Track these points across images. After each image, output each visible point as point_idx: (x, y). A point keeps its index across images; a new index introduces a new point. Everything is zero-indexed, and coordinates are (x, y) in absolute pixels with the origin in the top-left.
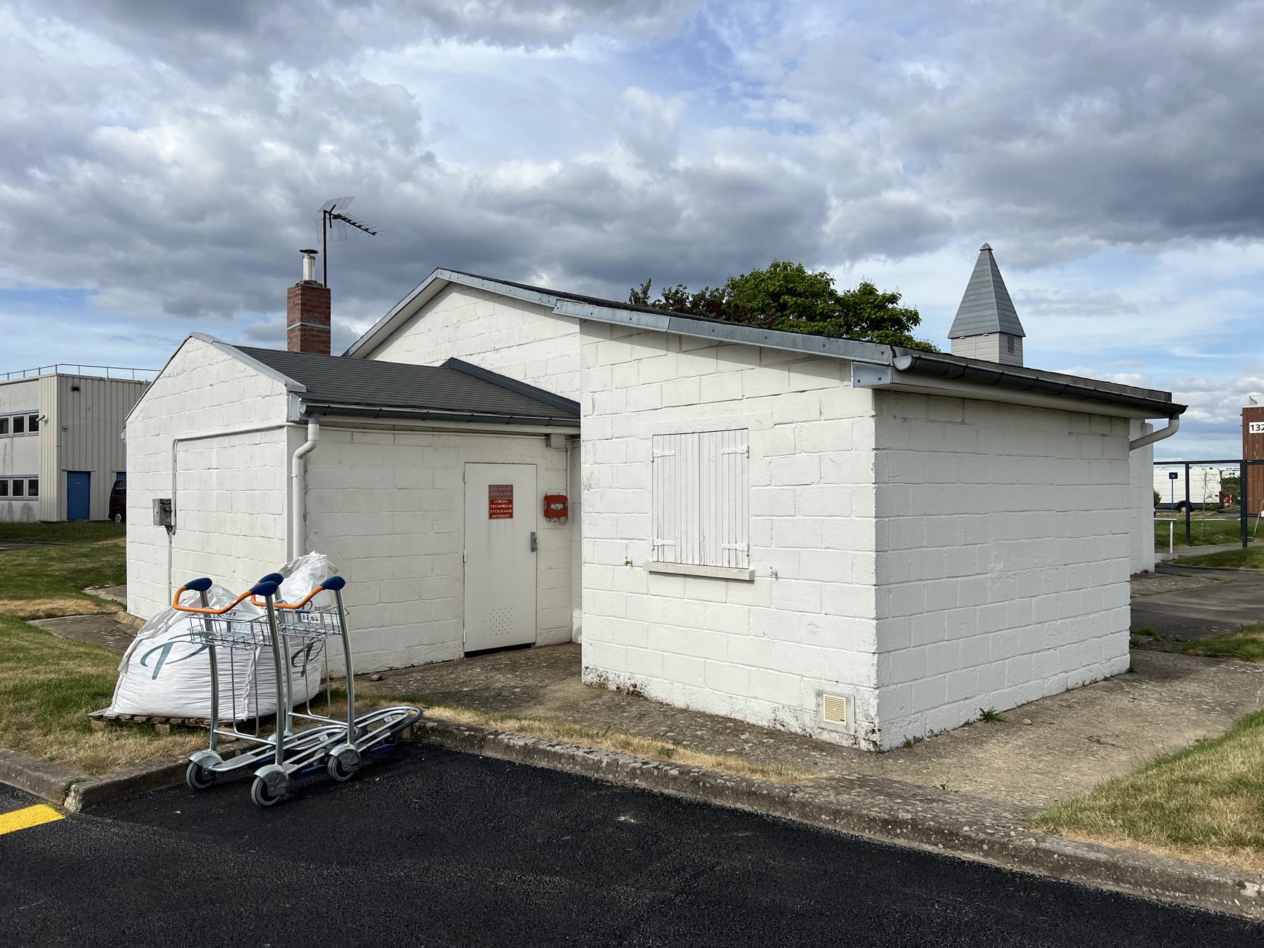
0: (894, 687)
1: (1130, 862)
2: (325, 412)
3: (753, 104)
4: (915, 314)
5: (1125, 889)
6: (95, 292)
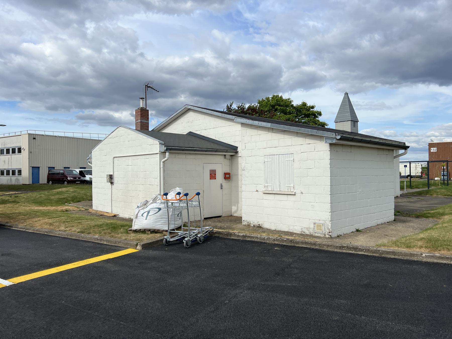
0: (335, 221)
1: (397, 251)
2: (171, 149)
3: (256, 36)
4: (320, 113)
5: (396, 257)
6: (20, 102)
